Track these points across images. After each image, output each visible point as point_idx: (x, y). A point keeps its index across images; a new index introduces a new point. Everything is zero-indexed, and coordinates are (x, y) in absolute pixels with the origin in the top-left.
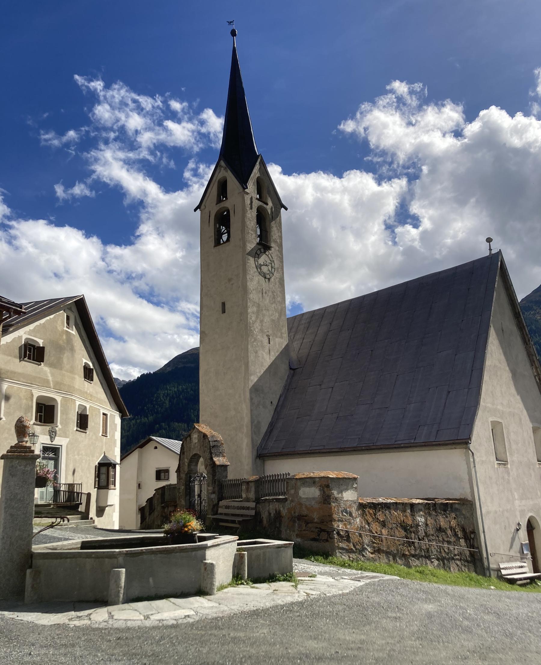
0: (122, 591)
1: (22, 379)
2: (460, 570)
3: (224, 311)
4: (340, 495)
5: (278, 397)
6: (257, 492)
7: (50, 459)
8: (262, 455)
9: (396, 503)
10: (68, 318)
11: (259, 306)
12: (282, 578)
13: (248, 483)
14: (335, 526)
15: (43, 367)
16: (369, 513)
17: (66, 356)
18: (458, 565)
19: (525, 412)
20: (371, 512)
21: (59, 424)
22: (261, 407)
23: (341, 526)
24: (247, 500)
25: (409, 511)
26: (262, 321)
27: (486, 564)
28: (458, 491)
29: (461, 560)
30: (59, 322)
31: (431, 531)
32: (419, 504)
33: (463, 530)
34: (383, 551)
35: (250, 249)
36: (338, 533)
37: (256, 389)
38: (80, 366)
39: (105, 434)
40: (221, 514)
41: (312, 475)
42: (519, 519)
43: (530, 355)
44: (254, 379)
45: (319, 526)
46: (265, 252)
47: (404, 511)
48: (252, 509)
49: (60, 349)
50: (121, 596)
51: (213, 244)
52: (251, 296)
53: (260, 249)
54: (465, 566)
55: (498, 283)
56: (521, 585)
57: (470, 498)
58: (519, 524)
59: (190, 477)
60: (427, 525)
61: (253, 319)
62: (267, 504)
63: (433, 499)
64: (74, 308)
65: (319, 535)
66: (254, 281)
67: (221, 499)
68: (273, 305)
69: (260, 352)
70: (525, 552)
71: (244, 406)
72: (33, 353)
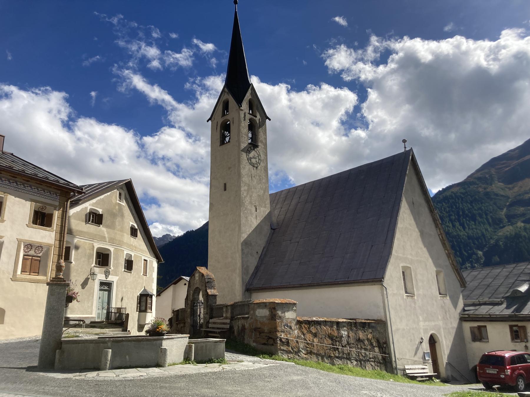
0: (109, 363)
1: (86, 236)
2: (374, 369)
3: (225, 190)
4: (283, 314)
5: (262, 248)
6: (232, 313)
7: (105, 290)
8: (250, 289)
9: (325, 321)
10: (120, 194)
11: (249, 186)
12: (217, 361)
13: (227, 306)
14: (279, 335)
15: (102, 228)
16: (305, 327)
17: (118, 220)
18: (372, 365)
19: (430, 260)
20: (306, 326)
21: (111, 267)
22: (249, 256)
23: (283, 336)
24: (226, 318)
25: (335, 327)
26: (251, 196)
27: (394, 365)
28: (376, 314)
29: (374, 362)
30: (114, 197)
31: (352, 341)
32: (343, 322)
33: (378, 341)
34: (314, 354)
35: (243, 147)
36: (281, 340)
37: (246, 243)
38: (127, 227)
39: (145, 273)
40: (211, 328)
41: (265, 301)
42: (423, 334)
43: (435, 220)
44: (244, 236)
45: (268, 335)
46: (254, 149)
47: (332, 327)
48: (228, 324)
49: (114, 215)
50: (108, 365)
51: (219, 144)
52: (244, 179)
53: (250, 147)
54: (378, 366)
55: (409, 169)
56: (420, 381)
57: (384, 319)
58: (422, 339)
59: (194, 303)
60: (349, 337)
61: (245, 194)
62: (237, 321)
63: (355, 319)
64: (125, 188)
65: (267, 341)
66: (246, 169)
67: (211, 318)
68: (260, 185)
69: (249, 218)
70: (427, 358)
71: (237, 255)
72: (96, 218)
